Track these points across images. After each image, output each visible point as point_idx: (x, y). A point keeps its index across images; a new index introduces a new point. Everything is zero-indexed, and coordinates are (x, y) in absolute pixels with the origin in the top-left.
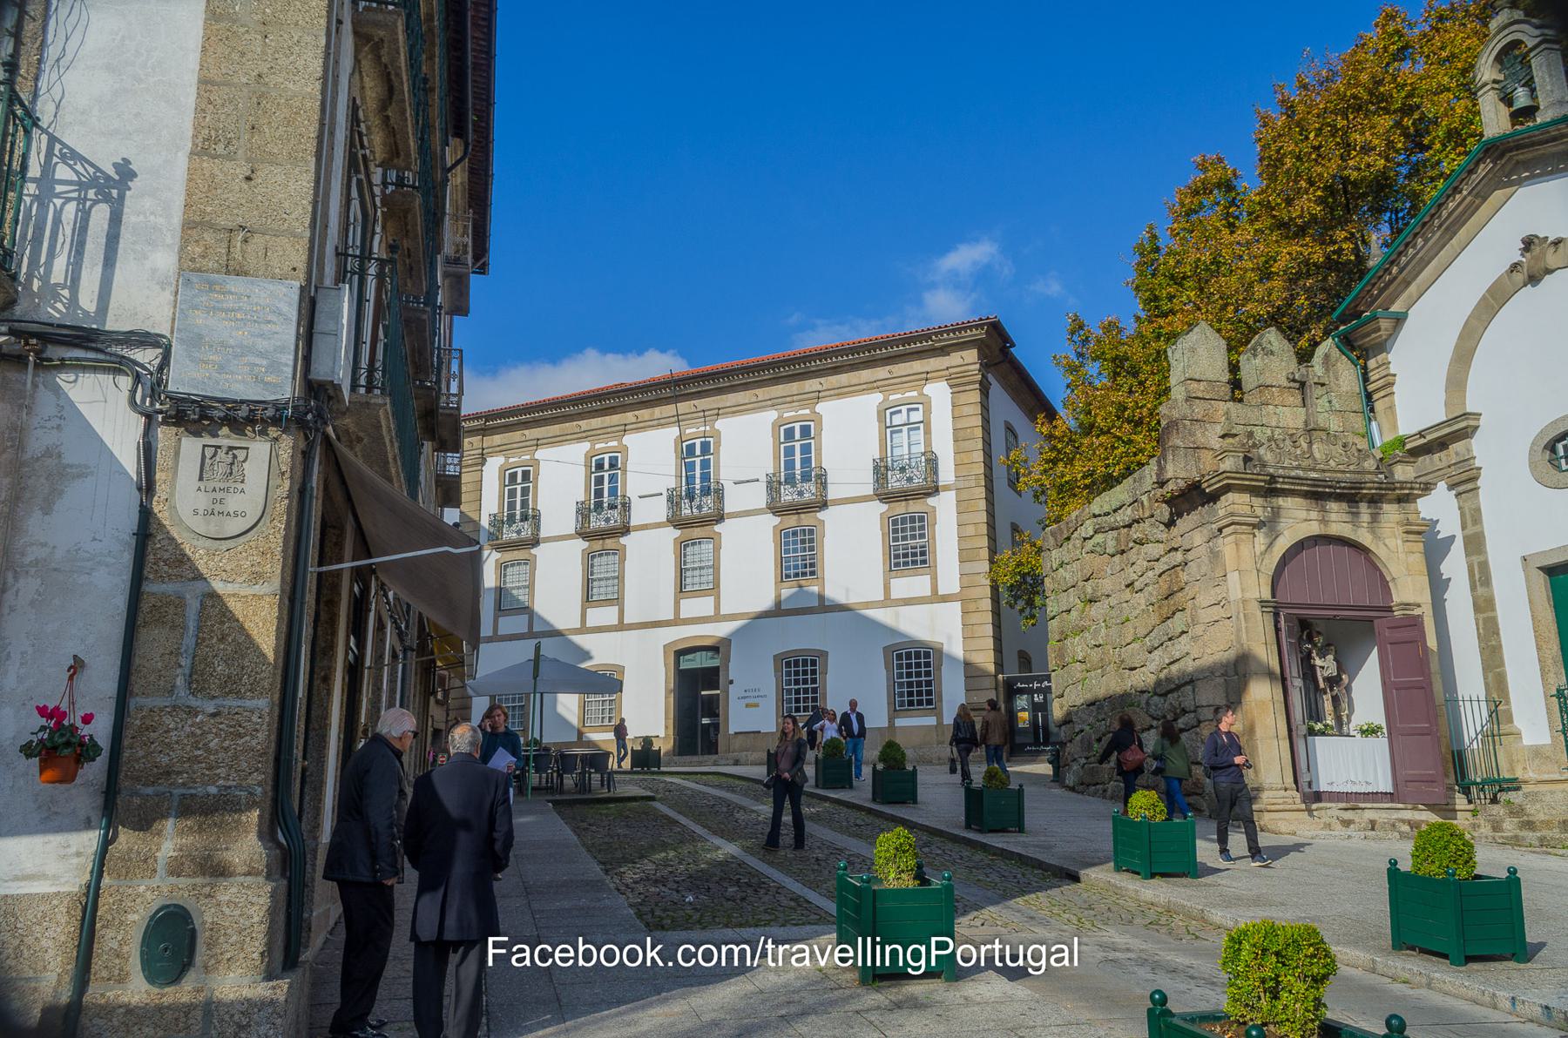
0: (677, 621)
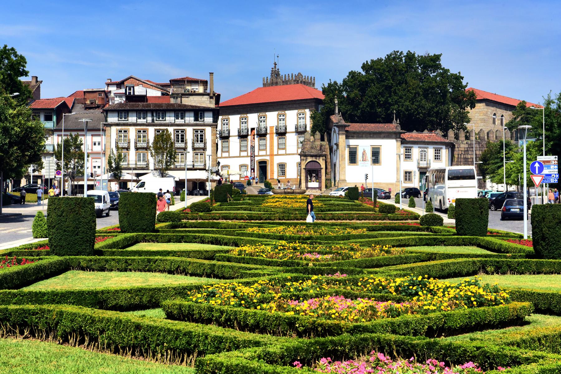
0: (240, 157)
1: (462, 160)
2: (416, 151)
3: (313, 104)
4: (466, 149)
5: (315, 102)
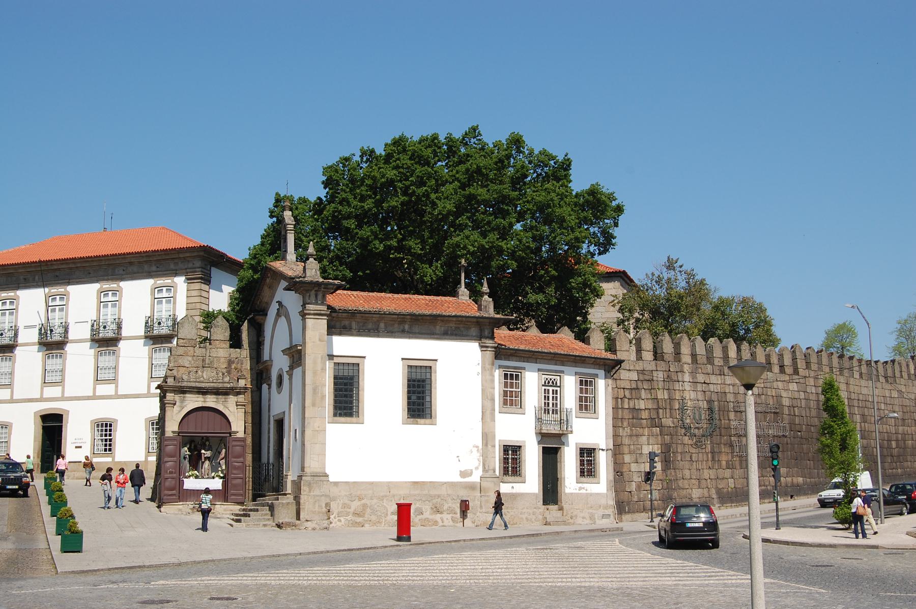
0: (94, 397)
1: (627, 415)
2: (532, 380)
3: (198, 263)
4: (634, 386)
5: (203, 259)
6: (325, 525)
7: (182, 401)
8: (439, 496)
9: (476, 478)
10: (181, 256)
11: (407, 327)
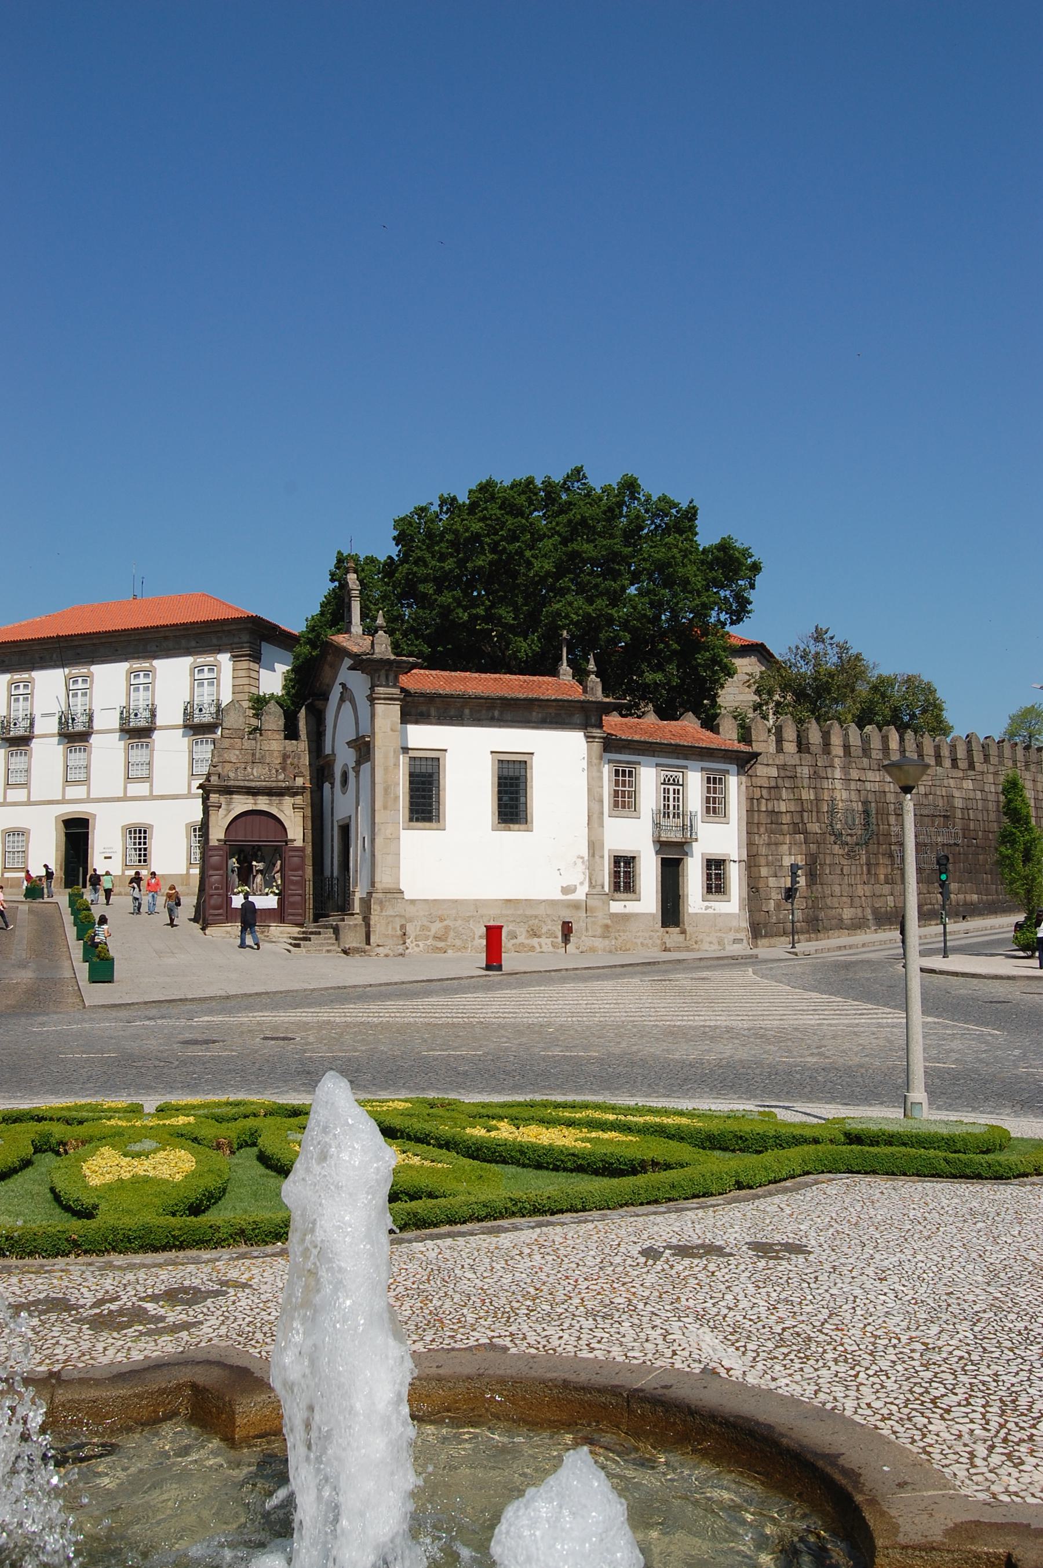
0: (125, 798)
2: (648, 778)
3: (245, 637)
4: (773, 784)
6: (401, 951)
7: (229, 803)
8: (536, 917)
9: (580, 894)
10: (226, 628)
11: (496, 713)
